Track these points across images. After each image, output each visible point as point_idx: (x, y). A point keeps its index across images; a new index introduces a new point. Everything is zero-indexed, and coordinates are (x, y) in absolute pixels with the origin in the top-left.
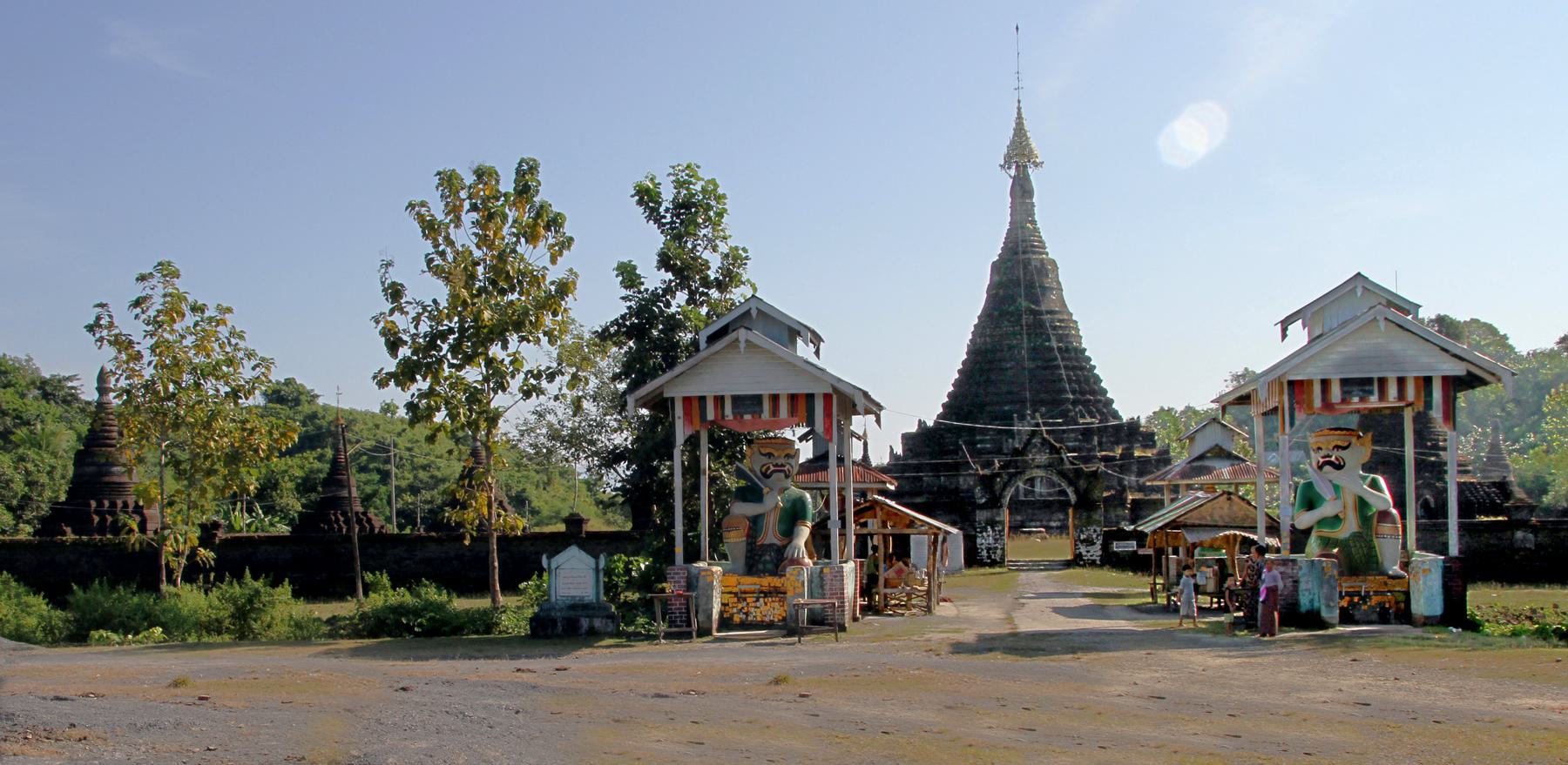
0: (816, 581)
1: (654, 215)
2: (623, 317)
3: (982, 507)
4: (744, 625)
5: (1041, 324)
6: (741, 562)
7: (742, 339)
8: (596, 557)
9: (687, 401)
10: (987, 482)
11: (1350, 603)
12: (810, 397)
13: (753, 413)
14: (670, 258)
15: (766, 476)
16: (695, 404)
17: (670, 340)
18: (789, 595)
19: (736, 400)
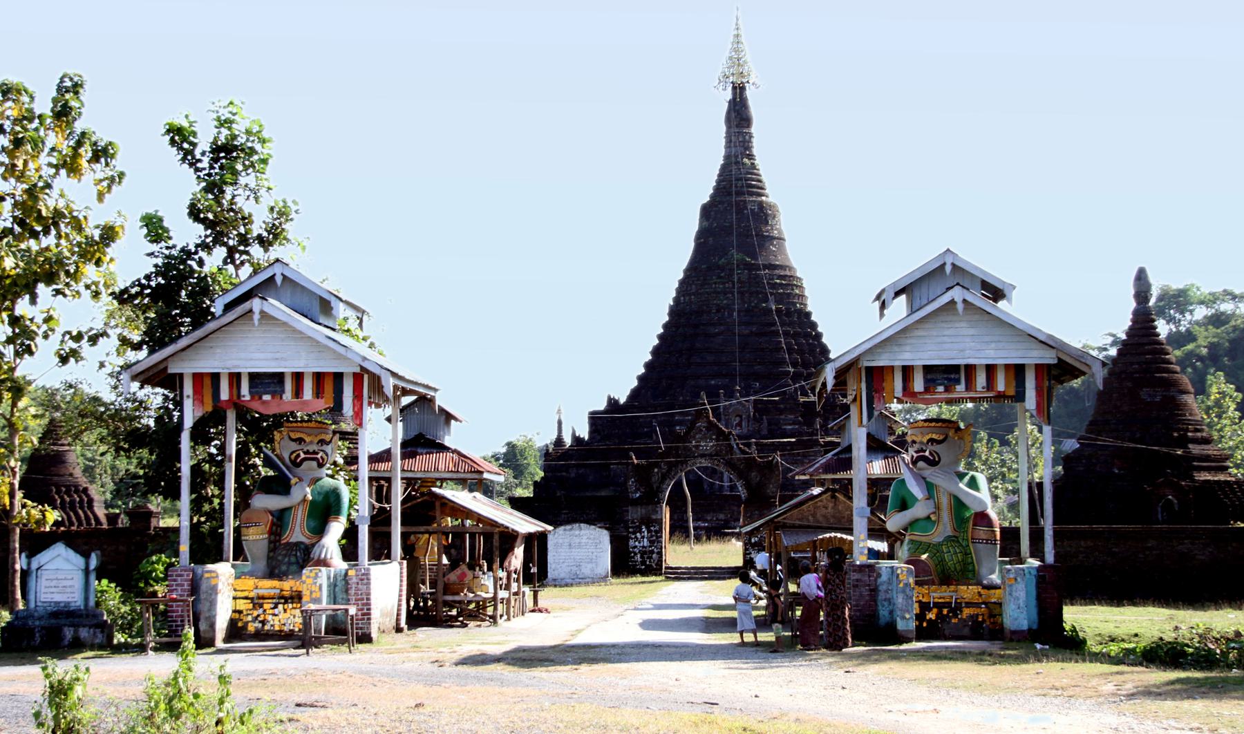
0: (340, 584)
1: (189, 157)
2: (148, 277)
3: (635, 503)
4: (260, 636)
5: (757, 280)
6: (262, 565)
7: (256, 309)
8: (86, 556)
9: (198, 378)
10: (643, 474)
11: (939, 615)
12: (338, 377)
13: (273, 395)
14: (200, 211)
15: (296, 464)
16: (207, 382)
17: (198, 304)
18: (305, 599)
19: (254, 377)
